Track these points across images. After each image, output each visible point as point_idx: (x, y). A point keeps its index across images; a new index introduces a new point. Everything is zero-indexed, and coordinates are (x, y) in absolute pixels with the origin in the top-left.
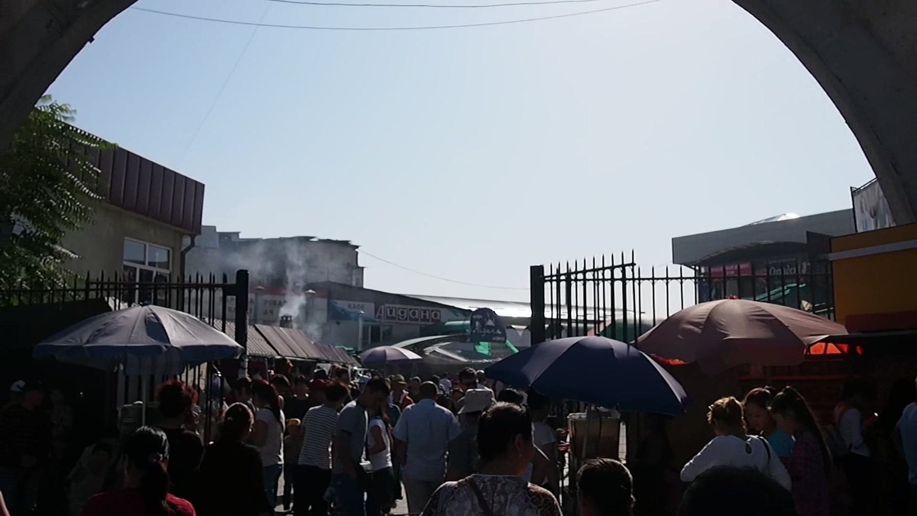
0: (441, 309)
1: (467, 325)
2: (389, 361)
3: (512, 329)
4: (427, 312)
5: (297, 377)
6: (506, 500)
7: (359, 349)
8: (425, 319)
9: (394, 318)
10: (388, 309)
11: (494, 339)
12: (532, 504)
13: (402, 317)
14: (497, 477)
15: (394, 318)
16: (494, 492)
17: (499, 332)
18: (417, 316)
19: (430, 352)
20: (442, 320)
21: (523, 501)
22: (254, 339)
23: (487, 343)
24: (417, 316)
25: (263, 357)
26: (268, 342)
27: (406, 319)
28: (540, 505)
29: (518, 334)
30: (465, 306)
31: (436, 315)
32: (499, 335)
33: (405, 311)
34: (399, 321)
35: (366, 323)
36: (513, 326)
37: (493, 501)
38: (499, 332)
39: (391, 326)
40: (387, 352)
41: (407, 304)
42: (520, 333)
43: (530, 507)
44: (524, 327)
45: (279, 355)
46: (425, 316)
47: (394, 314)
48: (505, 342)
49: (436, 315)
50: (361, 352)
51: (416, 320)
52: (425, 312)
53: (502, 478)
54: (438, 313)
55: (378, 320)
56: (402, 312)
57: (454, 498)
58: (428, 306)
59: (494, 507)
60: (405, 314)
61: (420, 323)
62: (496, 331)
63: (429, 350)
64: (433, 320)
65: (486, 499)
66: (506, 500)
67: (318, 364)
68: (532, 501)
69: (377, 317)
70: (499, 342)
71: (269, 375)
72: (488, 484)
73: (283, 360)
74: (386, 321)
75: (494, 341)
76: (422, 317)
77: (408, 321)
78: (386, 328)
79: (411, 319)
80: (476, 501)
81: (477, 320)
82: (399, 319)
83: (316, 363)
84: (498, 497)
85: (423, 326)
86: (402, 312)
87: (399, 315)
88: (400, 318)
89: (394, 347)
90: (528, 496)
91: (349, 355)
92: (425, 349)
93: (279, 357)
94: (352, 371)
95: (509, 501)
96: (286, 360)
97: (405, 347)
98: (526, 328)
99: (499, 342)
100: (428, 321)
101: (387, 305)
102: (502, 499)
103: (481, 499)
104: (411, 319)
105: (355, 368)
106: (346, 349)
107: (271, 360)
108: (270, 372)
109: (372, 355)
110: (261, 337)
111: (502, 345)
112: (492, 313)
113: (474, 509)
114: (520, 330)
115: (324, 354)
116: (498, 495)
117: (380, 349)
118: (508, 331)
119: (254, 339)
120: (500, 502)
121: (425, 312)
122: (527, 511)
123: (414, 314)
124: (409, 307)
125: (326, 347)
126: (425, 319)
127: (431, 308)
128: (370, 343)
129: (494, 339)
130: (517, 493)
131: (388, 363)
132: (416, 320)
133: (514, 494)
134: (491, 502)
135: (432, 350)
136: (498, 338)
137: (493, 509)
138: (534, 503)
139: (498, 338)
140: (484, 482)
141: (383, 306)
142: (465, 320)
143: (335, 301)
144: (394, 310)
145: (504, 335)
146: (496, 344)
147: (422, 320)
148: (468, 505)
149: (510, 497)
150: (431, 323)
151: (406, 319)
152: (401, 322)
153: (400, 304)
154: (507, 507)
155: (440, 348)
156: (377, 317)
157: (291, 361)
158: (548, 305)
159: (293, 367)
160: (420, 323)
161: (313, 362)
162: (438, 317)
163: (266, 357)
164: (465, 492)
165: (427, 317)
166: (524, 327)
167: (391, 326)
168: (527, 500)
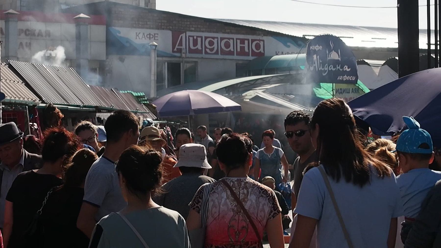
0: (265, 38)
1: (301, 60)
2: (194, 110)
3: (367, 66)
4: (246, 42)
5: (233, 93)
6: (248, 192)
7: (153, 95)
8: (242, 52)
9: (200, 52)
10: (191, 39)
11: (340, 78)
12: (263, 195)
13: (212, 50)
14: (240, 179)
15: (200, 52)
16: (240, 188)
17: (346, 68)
18: (231, 48)
19: (251, 97)
20: (267, 54)
21: (258, 193)
22: (8, 81)
23: (330, 85)
24: (231, 48)
25: (23, 105)
26: (28, 85)
27: (217, 53)
28: (267, 196)
29: (373, 72)
30: (298, 33)
31: (258, 46)
32: (348, 74)
33: (215, 41)
34: (207, 56)
35: (160, 59)
36: (366, 61)
37: (239, 192)
38: (346, 68)
39: (196, 62)
40: (191, 98)
41: (217, 32)
42: (377, 71)
43: (262, 196)
44: (382, 62)
45: (43, 102)
46: (242, 48)
47: (199, 46)
48: (355, 82)
49: (258, 46)
50: (155, 99)
51: (231, 53)
52: (242, 41)
53: (243, 179)
54: (261, 43)
55: (178, 55)
56: (211, 43)
57: (215, 192)
58: (247, 34)
59: (240, 197)
60: (215, 45)
61: (235, 57)
62: (342, 67)
63: (250, 94)
64: (254, 54)
65: (235, 191)
66: (248, 192)
67: (98, 115)
68: (263, 193)
69: (175, 50)
70: (348, 82)
71: (31, 129)
72: (236, 183)
73: (50, 109)
74: (188, 55)
75: (342, 82)
76: (239, 50)
77: (220, 56)
78: (188, 65)
79: (223, 53)
80: (229, 193)
81: (315, 52)
82: (206, 53)
83: (96, 112)
84: (242, 190)
85: (240, 62)
86: (211, 43)
87: (206, 47)
88: (208, 50)
89: (202, 90)
90: (260, 190)
91: (139, 102)
92: (243, 94)
93: (44, 105)
94: (144, 123)
95: (249, 194)
96: (54, 108)
97: (216, 92)
98: (384, 64)
99: (348, 82)
100: (247, 54)
101: (188, 33)
102: (245, 191)
103: (232, 191)
104: (223, 53)
105: (150, 120)
106: (135, 94)
107: (33, 108)
108: (33, 125)
109: (169, 103)
110: (17, 79)
111: (351, 87)
112: (337, 41)
113: (228, 198)
114: (377, 66)
115: (106, 103)
116: (243, 189)
117: (181, 94)
118: (359, 68)
119: (8, 81)
120: (244, 193)
121: (242, 41)
122: (260, 198)
123: (227, 45)
124: (220, 35)
125: (108, 92)
126: (242, 52)
127: (250, 37)
128: (166, 87)
129: (340, 78)
130: (254, 188)
131: (192, 114)
132: (231, 53)
133: (253, 189)
134: (238, 193)
135: (253, 96)
136: (346, 78)
137: (240, 197)
138: (264, 194)
139: (346, 78)
140: (233, 182)
141: (183, 35)
142: (300, 53)
143: (117, 28)
144: (199, 40)
145: (354, 73)
146: (344, 86)
147: (238, 54)
148: (224, 195)
149: (250, 190)
150: (251, 58)
151: (217, 53)
152: (207, 56)
153: (208, 32)
154: (249, 196)
155: (264, 92)
156: (175, 50)
157: (62, 110)
158: (423, 31)
159: (63, 119)
160: (235, 57)
161: (90, 112)
162: (261, 50)
163: (27, 105)
164: (221, 188)
165: (246, 50)
166: (382, 62)
167: (196, 62)
168: (260, 193)
